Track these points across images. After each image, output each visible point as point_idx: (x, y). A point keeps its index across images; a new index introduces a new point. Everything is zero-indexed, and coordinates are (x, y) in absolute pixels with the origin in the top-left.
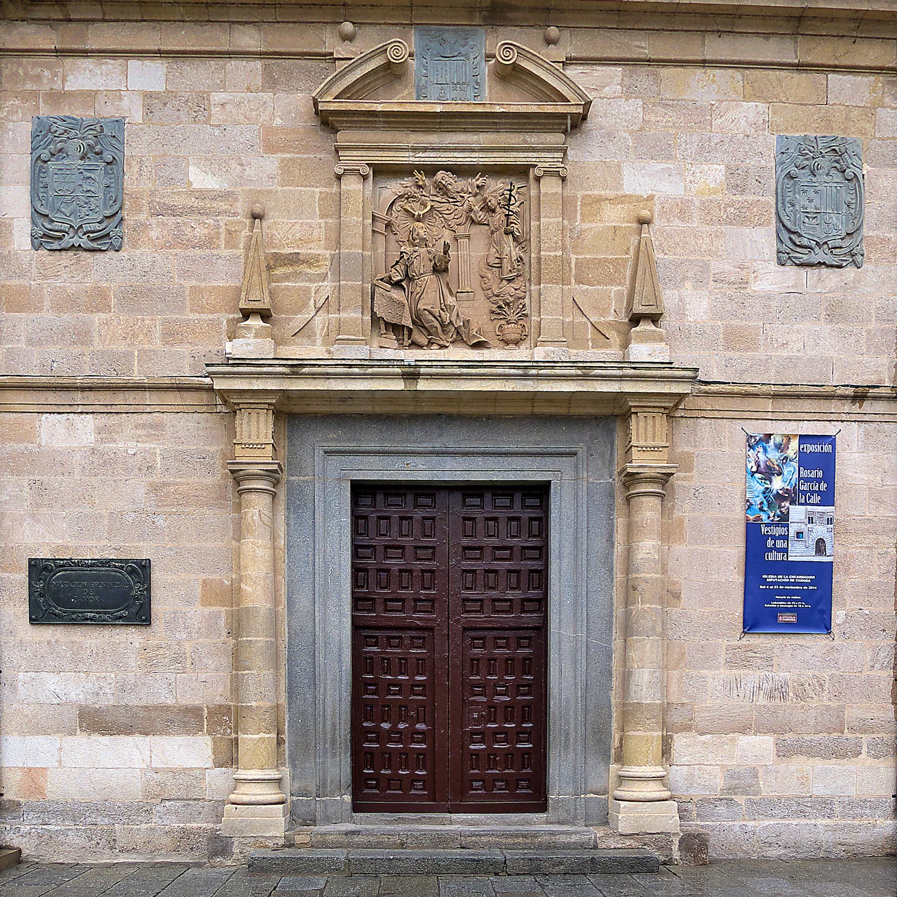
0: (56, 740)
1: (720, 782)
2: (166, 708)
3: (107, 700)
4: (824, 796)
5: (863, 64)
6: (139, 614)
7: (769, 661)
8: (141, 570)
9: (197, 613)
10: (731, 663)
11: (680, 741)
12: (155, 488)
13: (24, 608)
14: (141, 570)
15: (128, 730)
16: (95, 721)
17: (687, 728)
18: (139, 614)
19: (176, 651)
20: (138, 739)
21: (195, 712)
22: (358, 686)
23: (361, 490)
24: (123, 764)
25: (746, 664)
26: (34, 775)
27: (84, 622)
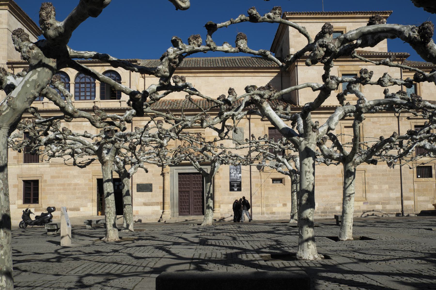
0: (140, 207)
1: (227, 211)
2: (154, 202)
3: (147, 201)
4: (191, 1)
5: (19, 6)
6: (151, 191)
7: (233, 195)
8: (151, 185)
9: (158, 190)
10: (228, 195)
11: (221, 205)
12: (153, 174)
13: (136, 190)
14: (151, 185)
15: (149, 205)
16: (145, 204)
17: (222, 204)
18: (151, 191)
19: (156, 195)
20: (151, 206)
21: (158, 203)
22: (180, 196)
23: (179, 174)
24: (149, 209)
25: (230, 195)
26: (137, 212)
27: (144, 191)
